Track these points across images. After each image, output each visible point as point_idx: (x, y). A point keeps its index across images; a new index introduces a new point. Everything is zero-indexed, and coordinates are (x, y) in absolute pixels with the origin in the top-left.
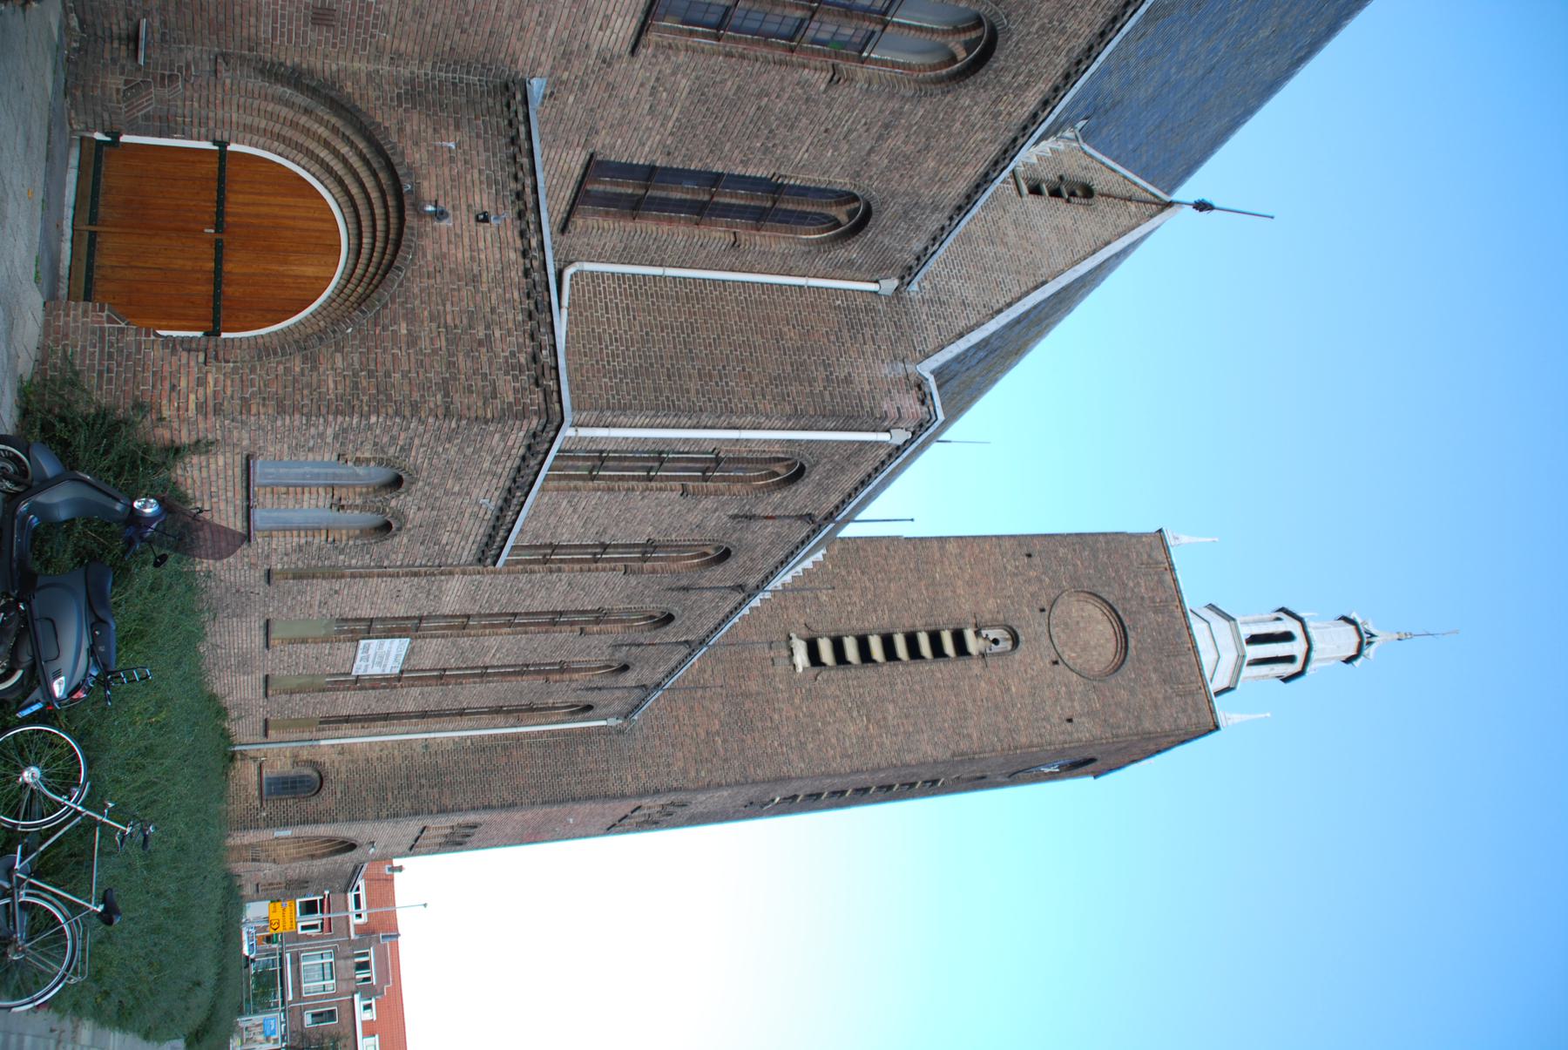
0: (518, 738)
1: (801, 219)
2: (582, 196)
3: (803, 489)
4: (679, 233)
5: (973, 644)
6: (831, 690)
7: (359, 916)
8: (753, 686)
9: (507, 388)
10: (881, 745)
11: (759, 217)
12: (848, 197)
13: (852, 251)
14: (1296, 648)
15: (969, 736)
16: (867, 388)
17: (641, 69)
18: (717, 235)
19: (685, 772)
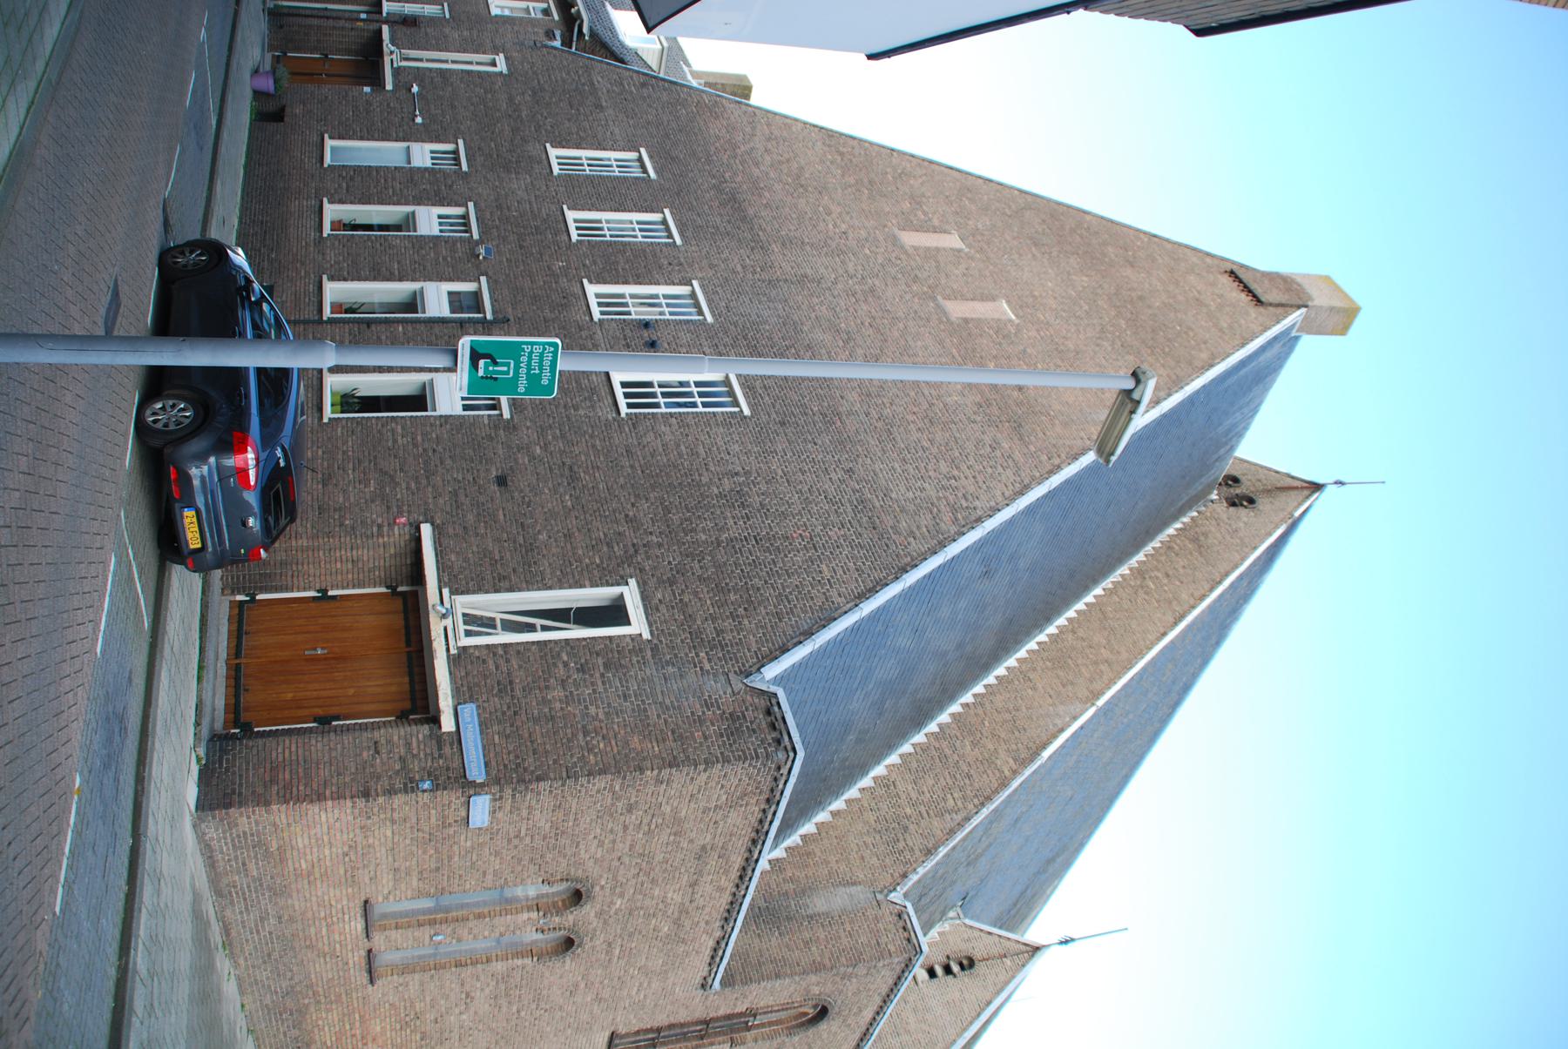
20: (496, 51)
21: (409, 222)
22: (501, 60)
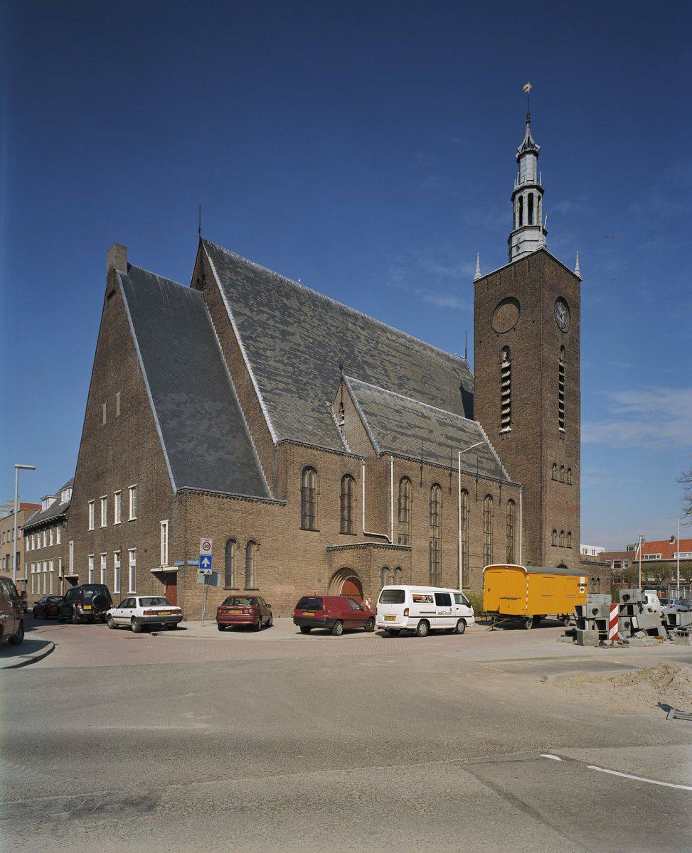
0: (523, 520)
1: (350, 489)
2: (349, 533)
3: (410, 474)
4: (354, 512)
5: (506, 365)
6: (517, 418)
7: (658, 556)
8: (514, 446)
9: (367, 552)
10: (535, 399)
11: (350, 495)
12: (343, 481)
13: (355, 475)
14: (525, 194)
15: (535, 364)
16: (154, 831)
17: (323, 530)
18: (354, 504)
19: (536, 468)
20: (68, 544)
21: (104, 570)
22: (163, 522)
